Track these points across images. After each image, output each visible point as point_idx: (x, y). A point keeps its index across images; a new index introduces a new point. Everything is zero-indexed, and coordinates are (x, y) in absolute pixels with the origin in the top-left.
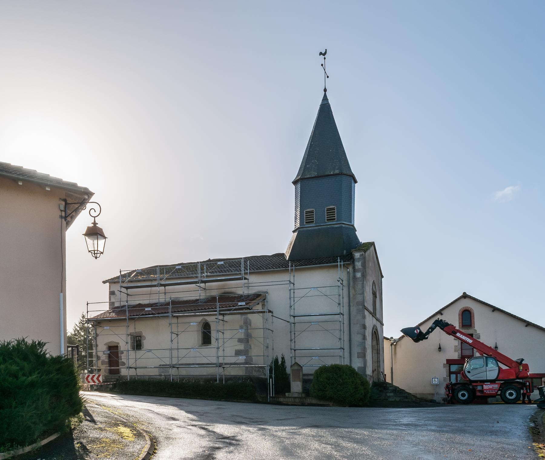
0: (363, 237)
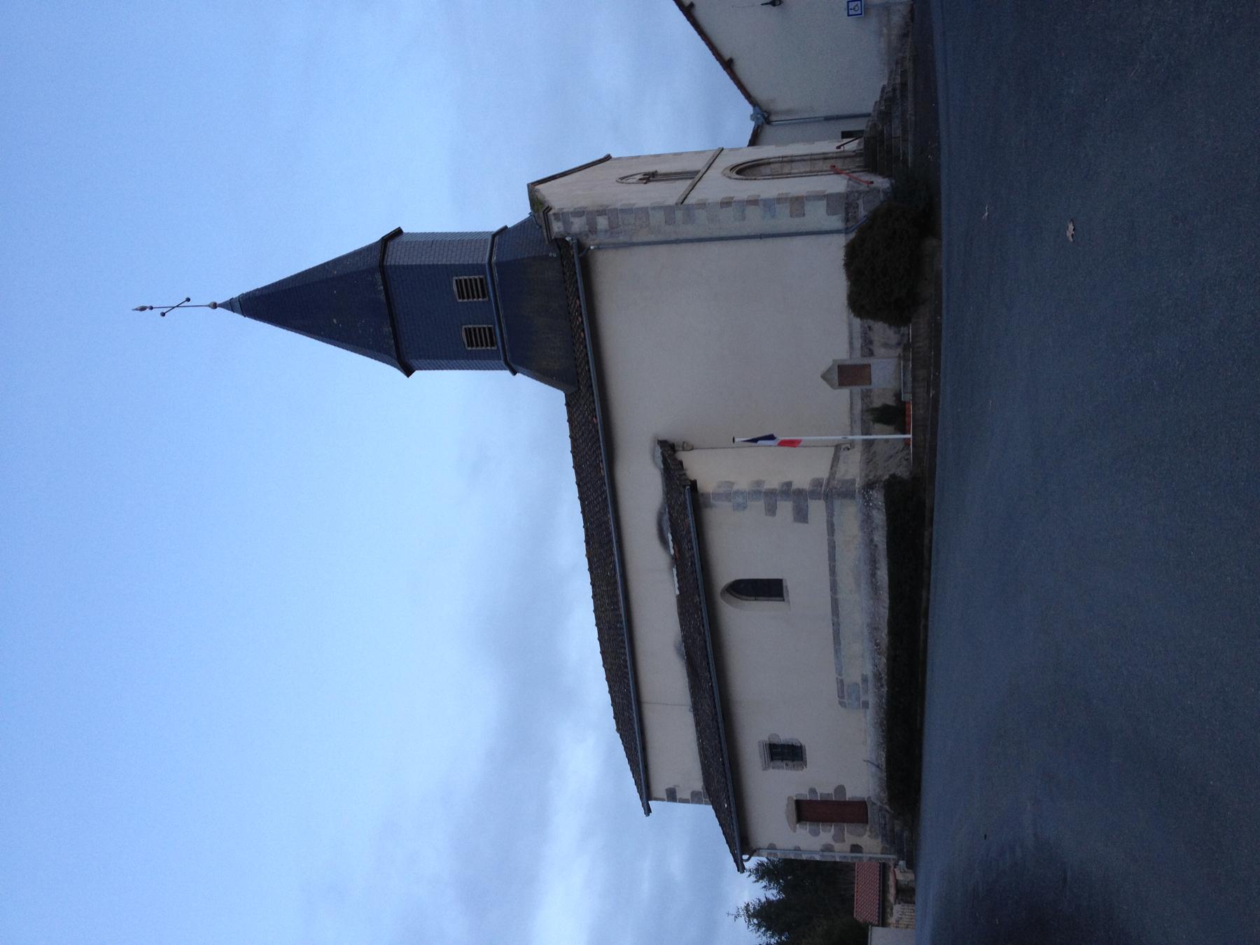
0: (516, 212)
